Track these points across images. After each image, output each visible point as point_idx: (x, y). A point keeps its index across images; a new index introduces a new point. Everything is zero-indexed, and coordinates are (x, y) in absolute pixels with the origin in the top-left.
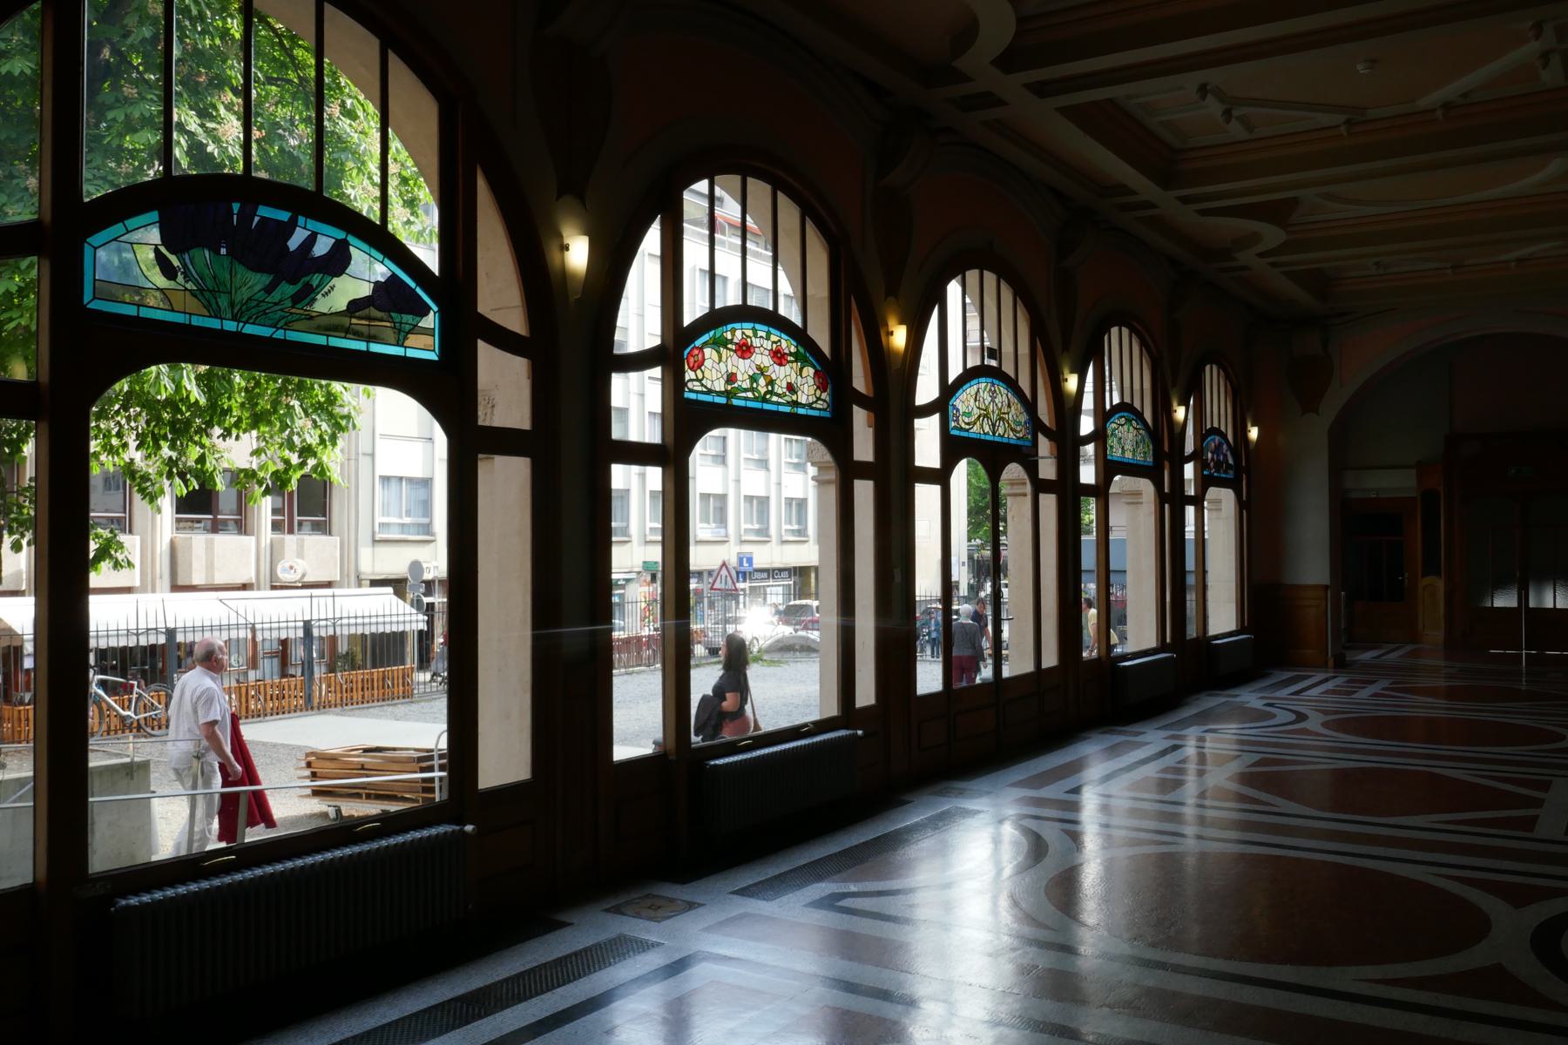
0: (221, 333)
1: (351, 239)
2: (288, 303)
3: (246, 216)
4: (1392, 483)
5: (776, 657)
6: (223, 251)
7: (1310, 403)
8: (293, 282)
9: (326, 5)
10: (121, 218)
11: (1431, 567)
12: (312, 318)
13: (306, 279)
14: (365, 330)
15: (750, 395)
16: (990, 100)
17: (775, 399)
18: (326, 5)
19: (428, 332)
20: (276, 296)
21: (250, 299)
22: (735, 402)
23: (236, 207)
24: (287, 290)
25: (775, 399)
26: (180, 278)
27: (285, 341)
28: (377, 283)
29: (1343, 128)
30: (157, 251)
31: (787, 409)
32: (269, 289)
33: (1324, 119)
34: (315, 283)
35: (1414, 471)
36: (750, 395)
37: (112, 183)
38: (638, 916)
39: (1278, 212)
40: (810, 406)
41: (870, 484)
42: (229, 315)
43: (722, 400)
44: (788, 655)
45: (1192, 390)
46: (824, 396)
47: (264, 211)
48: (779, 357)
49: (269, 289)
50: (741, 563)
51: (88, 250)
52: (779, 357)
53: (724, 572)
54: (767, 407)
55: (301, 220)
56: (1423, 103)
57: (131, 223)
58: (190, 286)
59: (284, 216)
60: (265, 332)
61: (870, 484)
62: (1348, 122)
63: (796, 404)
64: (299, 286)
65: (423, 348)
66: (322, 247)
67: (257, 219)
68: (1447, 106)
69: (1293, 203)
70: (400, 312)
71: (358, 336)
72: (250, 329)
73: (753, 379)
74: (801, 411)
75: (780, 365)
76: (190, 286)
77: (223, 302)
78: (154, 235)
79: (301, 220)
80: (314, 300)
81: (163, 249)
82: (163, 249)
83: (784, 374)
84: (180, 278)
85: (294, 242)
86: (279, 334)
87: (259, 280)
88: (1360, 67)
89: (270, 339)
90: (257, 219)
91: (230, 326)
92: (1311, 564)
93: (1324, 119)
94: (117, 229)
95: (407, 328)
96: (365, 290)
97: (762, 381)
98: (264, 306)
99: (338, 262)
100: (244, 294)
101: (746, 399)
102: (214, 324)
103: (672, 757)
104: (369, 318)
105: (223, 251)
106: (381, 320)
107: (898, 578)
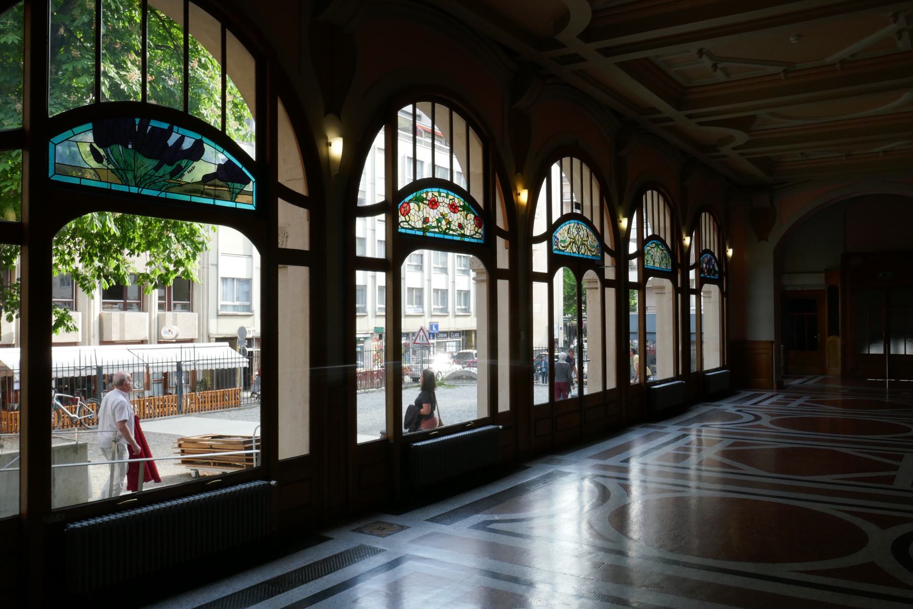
0: (129, 194)
1: (204, 139)
2: (168, 177)
3: (143, 126)
4: (810, 281)
5: (452, 383)
6: (130, 146)
7: (763, 235)
8: (171, 164)
9: (190, 3)
10: (70, 127)
11: (833, 331)
12: (181, 185)
13: (178, 163)
14: (212, 192)
15: (437, 230)
16: (576, 58)
17: (451, 232)
18: (190, 3)
19: (249, 193)
20: (161, 172)
21: (145, 174)
22: (428, 234)
23: (137, 120)
24: (167, 169)
25: (451, 232)
26: (105, 162)
27: (166, 199)
28: (219, 165)
29: (782, 75)
30: (91, 146)
31: (458, 239)
32: (157, 169)
33: (771, 69)
34: (183, 165)
35: (823, 275)
36: (437, 230)
37: (65, 107)
38: (371, 534)
39: (744, 124)
40: (471, 236)
41: (506, 282)
42: (133, 184)
43: (420, 233)
44: (459, 382)
45: (694, 227)
46: (480, 231)
47: (154, 123)
48: (453, 208)
49: (157, 169)
50: (431, 328)
51: (51, 146)
52: (453, 208)
53: (422, 333)
54: (446, 237)
55: (175, 128)
56: (829, 60)
57: (76, 130)
58: (110, 166)
59: (165, 126)
60: (154, 193)
61: (506, 282)
62: (785, 71)
63: (463, 235)
64: (174, 167)
65: (246, 203)
66: (187, 144)
67: (149, 128)
68: (843, 62)
69: (753, 118)
70: (233, 182)
71: (209, 196)
72: (145, 192)
73: (438, 221)
74: (467, 240)
75: (454, 212)
76: (110, 166)
77: (130, 176)
78: (90, 137)
79: (175, 128)
80: (183, 175)
81: (95, 145)
82: (95, 145)
83: (456, 218)
84: (105, 162)
85: (171, 141)
86: (163, 195)
87: (151, 163)
88: (792, 39)
89: (157, 198)
90: (149, 128)
91: (134, 190)
92: (763, 329)
93: (771, 69)
94: (68, 133)
95: (237, 191)
96: (213, 169)
97: (444, 222)
98: (154, 178)
99: (197, 153)
100: (142, 171)
101: (435, 232)
102: (125, 189)
103: (392, 441)
104: (215, 186)
105: (130, 146)
106: (222, 186)
107: (523, 337)
